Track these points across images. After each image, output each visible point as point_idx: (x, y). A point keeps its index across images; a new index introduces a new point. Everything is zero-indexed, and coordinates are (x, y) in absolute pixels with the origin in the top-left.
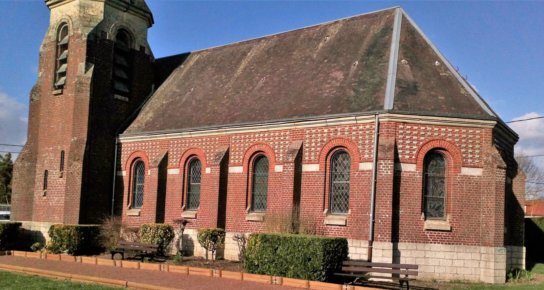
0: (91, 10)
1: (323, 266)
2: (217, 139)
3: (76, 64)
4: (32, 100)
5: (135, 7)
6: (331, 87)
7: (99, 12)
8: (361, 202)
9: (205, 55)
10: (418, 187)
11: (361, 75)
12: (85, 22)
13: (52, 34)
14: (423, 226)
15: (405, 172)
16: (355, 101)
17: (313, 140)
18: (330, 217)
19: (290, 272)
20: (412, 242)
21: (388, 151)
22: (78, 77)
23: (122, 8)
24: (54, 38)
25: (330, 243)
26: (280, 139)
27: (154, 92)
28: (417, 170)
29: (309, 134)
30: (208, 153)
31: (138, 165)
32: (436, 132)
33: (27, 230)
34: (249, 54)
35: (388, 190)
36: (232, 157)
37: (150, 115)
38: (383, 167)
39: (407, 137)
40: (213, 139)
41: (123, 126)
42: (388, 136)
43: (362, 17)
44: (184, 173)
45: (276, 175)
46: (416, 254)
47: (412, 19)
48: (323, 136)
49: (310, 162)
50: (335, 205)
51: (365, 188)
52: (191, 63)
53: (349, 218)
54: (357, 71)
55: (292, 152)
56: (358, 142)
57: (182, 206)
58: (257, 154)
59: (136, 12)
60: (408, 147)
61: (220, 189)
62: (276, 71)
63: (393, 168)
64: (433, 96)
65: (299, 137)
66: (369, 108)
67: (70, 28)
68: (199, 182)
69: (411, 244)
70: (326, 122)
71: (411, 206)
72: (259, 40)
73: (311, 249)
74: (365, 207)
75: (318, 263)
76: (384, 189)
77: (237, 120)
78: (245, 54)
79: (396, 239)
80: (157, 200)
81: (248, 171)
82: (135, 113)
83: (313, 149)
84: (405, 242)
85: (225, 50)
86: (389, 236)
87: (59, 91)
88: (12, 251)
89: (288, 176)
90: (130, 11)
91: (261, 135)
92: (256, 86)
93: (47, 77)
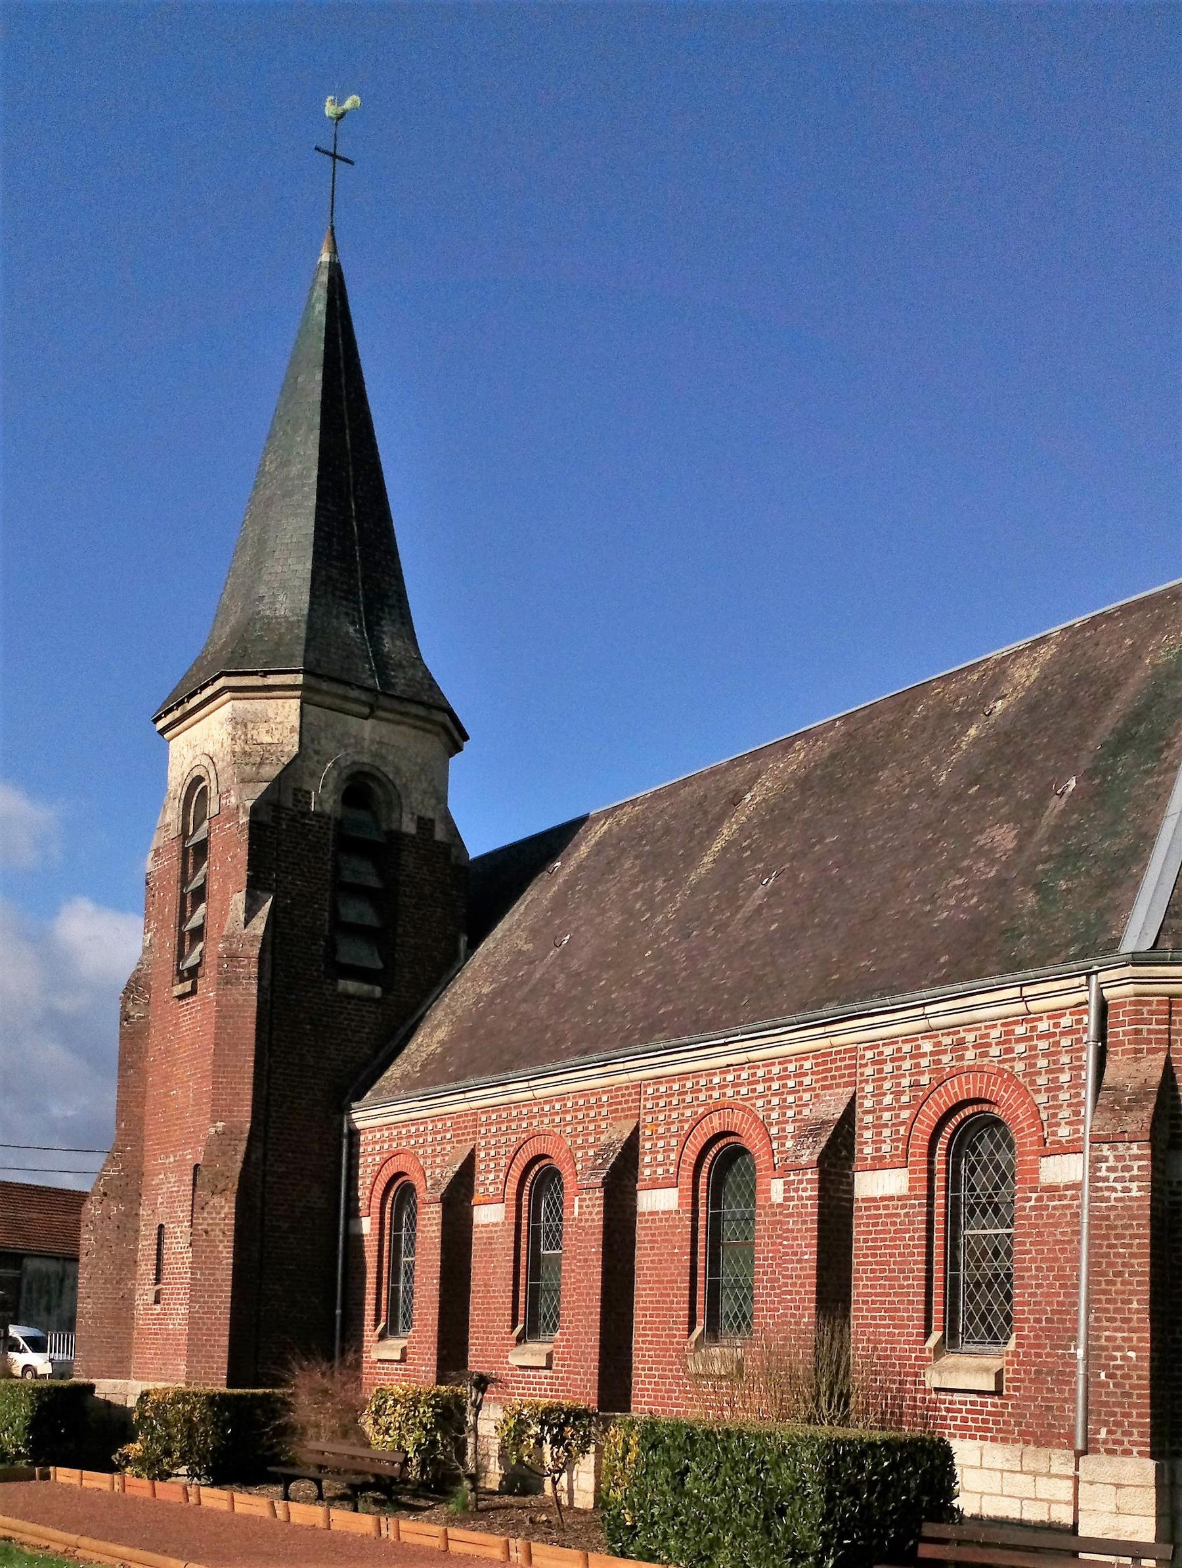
0: (263, 727)
1: (824, 1535)
2: (605, 1098)
3: (226, 900)
4: (126, 1017)
5: (398, 698)
6: (966, 886)
7: (286, 732)
8: (1049, 1303)
9: (625, 819)
11: (1078, 827)
12: (248, 768)
13: (172, 815)
16: (1033, 930)
17: (887, 1085)
18: (949, 1360)
21: (1129, 1109)
22: (227, 938)
24: (175, 830)
25: (863, 1454)
26: (785, 1086)
27: (467, 959)
30: (578, 1148)
31: (401, 1194)
33: (116, 1407)
34: (748, 796)
35: (1132, 1255)
36: (647, 1159)
37: (441, 1034)
38: (1109, 1169)
41: (359, 1080)
42: (1137, 1051)
43: (1126, 610)
45: (774, 1215)
48: (917, 1065)
49: (879, 1163)
50: (971, 1318)
52: (584, 850)
55: (815, 1129)
57: (514, 1327)
59: (402, 714)
61: (604, 1266)
62: (814, 845)
63: (1147, 1173)
65: (843, 1076)
66: (1072, 951)
67: (213, 793)
68: (558, 1246)
70: (925, 1017)
73: (786, 1473)
76: (1117, 1255)
77: (663, 1030)
78: (736, 799)
81: (930, 1205)
82: (402, 1031)
83: (887, 1115)
85: (684, 792)
86: (1141, 1434)
87: (187, 986)
88: (51, 1469)
89: (800, 1215)
90: (380, 713)
91: (730, 1077)
92: (741, 907)
93: (162, 947)
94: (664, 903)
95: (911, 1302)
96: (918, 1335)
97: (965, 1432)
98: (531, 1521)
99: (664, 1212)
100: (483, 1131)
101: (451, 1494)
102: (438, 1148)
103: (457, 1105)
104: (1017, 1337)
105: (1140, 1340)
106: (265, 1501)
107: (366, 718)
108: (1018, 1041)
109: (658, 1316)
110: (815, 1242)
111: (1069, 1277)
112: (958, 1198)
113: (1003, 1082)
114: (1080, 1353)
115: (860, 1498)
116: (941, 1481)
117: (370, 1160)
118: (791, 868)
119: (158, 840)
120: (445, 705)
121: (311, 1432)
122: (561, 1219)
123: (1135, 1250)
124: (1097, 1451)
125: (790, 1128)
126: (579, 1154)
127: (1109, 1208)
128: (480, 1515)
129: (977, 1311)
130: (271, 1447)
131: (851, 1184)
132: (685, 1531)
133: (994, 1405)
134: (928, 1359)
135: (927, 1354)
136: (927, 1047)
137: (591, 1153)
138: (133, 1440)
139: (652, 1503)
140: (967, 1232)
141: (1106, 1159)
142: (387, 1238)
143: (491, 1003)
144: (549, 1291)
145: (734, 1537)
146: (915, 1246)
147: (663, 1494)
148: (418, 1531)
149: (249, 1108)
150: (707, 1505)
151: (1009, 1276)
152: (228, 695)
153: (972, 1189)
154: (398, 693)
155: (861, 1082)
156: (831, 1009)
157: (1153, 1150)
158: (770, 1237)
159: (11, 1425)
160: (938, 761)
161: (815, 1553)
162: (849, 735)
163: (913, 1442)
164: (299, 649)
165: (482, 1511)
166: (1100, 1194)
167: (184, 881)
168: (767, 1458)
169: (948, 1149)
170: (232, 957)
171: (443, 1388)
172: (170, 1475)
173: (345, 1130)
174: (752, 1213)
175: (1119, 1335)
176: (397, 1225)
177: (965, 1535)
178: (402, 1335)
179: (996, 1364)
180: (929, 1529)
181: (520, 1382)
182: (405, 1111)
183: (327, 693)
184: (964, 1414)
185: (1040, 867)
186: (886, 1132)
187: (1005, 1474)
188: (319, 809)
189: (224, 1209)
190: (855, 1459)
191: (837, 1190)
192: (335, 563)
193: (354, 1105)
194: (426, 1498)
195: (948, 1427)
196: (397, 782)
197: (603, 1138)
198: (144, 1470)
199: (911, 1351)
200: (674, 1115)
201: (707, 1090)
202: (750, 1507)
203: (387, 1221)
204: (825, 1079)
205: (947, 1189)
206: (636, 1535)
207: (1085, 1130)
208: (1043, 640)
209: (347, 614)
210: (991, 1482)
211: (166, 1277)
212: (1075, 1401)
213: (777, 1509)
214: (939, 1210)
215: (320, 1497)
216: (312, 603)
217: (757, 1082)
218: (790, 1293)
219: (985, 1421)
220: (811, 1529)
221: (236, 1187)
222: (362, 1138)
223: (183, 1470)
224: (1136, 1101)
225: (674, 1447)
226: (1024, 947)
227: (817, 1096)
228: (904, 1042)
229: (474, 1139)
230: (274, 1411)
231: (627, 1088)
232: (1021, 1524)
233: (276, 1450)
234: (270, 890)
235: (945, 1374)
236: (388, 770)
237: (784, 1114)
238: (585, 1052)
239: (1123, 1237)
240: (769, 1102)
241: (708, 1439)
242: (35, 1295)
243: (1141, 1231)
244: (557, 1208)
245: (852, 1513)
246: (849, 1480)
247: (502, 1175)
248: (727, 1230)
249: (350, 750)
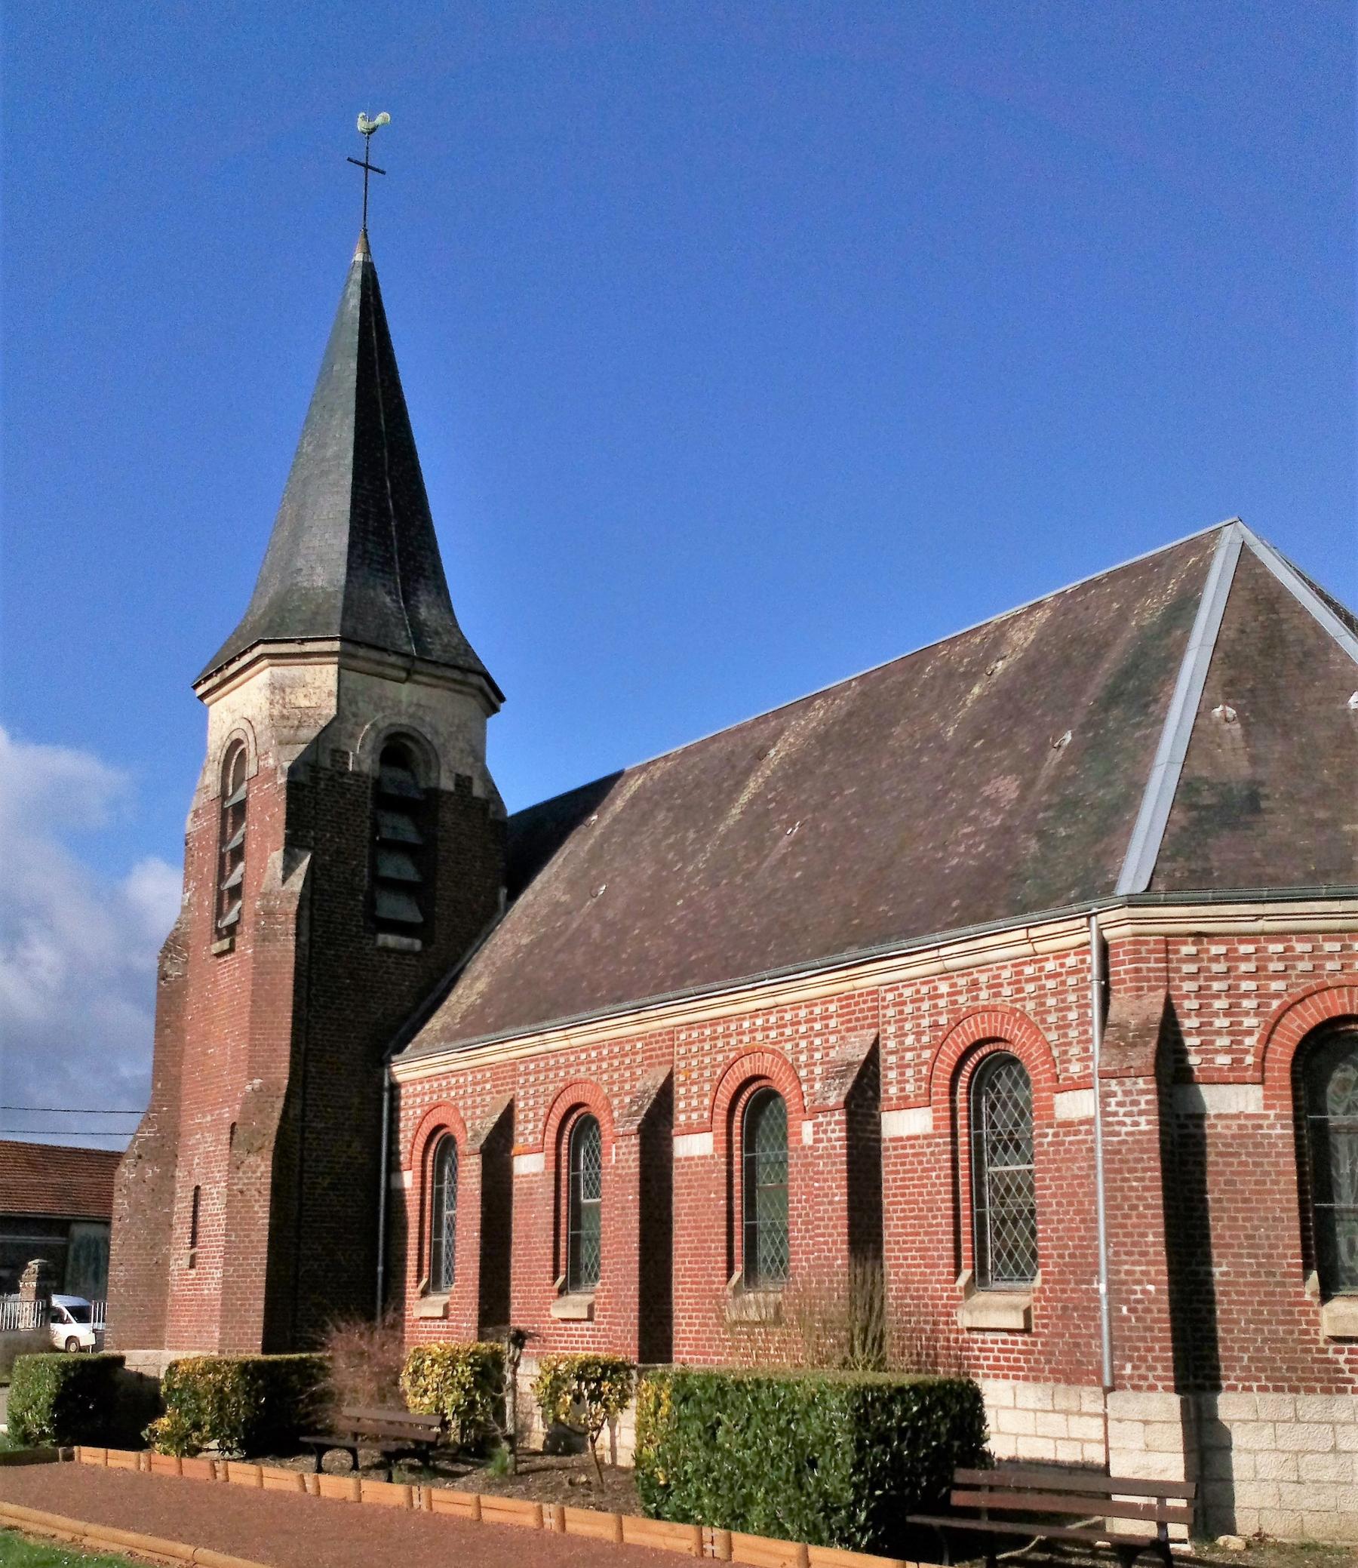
2: (639, 1045)
3: (264, 859)
4: (163, 976)
5: (434, 663)
6: (973, 834)
8: (1071, 1238)
9: (658, 774)
10: (1279, 1173)
13: (211, 778)
14: (1316, 1323)
15: (1219, 1116)
17: (908, 1026)
18: (980, 1298)
19: (756, 1515)
20: (1277, 1389)
21: (1134, 1045)
22: (265, 896)
23: (395, 673)
24: (215, 789)
25: (892, 1399)
26: (812, 1029)
27: (507, 910)
28: (1267, 1107)
29: (895, 1005)
31: (442, 1146)
32: (1331, 956)
34: (772, 752)
35: (1146, 1189)
36: (682, 1105)
37: (481, 986)
38: (1120, 1104)
39: (1216, 986)
40: (628, 1047)
41: (399, 1031)
44: (558, 1166)
45: (806, 1156)
46: (1293, 1437)
47: (1274, 547)
48: (935, 1006)
49: (905, 1104)
50: (999, 1256)
51: (1081, 1185)
52: (619, 804)
53: (1037, 1300)
54: (1061, 765)
56: (1043, 1021)
57: (555, 1278)
58: (752, 1088)
60: (1221, 1022)
62: (834, 797)
63: (1154, 1107)
64: (1322, 825)
65: (866, 1018)
66: (1073, 894)
67: (251, 755)
68: (598, 1195)
69: (1271, 1396)
71: (1259, 1247)
72: (808, 703)
75: (835, 1476)
76: (1131, 1189)
77: (693, 977)
78: (761, 755)
79: (1207, 1377)
80: (482, 1261)
81: (954, 1143)
82: (444, 983)
83: (909, 1055)
84: (1249, 1389)
85: (713, 748)
86: (1165, 1369)
87: (225, 944)
88: (76, 1448)
89: (829, 1156)
91: (759, 1022)
92: (767, 856)
93: (200, 905)
94: (694, 854)
95: (940, 1241)
96: (949, 1274)
97: (998, 1372)
98: (571, 1483)
99: (701, 1158)
100: (522, 1081)
101: (490, 1457)
102: (478, 1100)
103: (494, 1055)
104: (1043, 1273)
105: (1157, 1273)
106: (293, 1475)
107: (403, 682)
108: (1028, 981)
109: (696, 1262)
110: (844, 1183)
111: (1088, 1212)
112: (980, 1136)
113: (1016, 1021)
114: (1103, 1288)
115: (891, 1446)
116: (971, 1425)
117: (411, 1112)
118: (813, 819)
119: (198, 801)
120: (480, 669)
121: (348, 1397)
122: (600, 1167)
123: (1147, 1183)
124: (1123, 1387)
125: (818, 1070)
126: (616, 1102)
127: (1120, 1143)
128: (518, 1479)
129: (1027, 1240)
130: (308, 1415)
131: (879, 1124)
132: (718, 1488)
133: (1025, 1343)
134: (959, 1298)
135: (958, 1293)
136: (944, 988)
137: (627, 1100)
138: (161, 1413)
139: (685, 1459)
140: (991, 1169)
141: (1114, 1095)
142: (428, 1191)
143: (530, 953)
144: (590, 1240)
145: (767, 1493)
146: (942, 1185)
147: (695, 1449)
148: (451, 1500)
149: (287, 1064)
150: (739, 1460)
151: (1032, 1212)
152: (265, 662)
153: (994, 1126)
154: (434, 658)
155: (884, 1023)
156: (853, 953)
157: (1159, 1083)
158: (803, 1180)
159: (35, 1403)
160: (945, 717)
161: (847, 1507)
162: (864, 694)
163: (942, 1385)
164: (336, 618)
165: (522, 1473)
166: (1111, 1129)
167: (223, 841)
168: (797, 1407)
169: (969, 1088)
170: (269, 913)
171: (483, 1345)
172: (199, 1450)
173: (386, 1084)
174: (785, 1156)
175: (1138, 1268)
176: (439, 1177)
177: (996, 1481)
178: (444, 1290)
179: (1024, 1301)
180: (961, 1475)
181: (562, 1335)
182: (446, 1063)
184: (996, 1354)
185: (1041, 815)
186: (909, 1072)
187: (1039, 1414)
189: (262, 1167)
190: (884, 1406)
191: (865, 1131)
192: (370, 537)
193: (394, 1058)
194: (466, 1463)
195: (981, 1367)
197: (638, 1084)
198: (171, 1446)
199: (943, 1290)
200: (707, 1060)
201: (738, 1034)
202: (781, 1460)
203: (429, 1174)
204: (849, 1021)
205: (969, 1127)
206: (670, 1494)
207: (1094, 1066)
208: (1038, 605)
209: (384, 585)
210: (1024, 1423)
211: (201, 1240)
212: (1100, 1337)
213: (809, 1461)
214: (963, 1148)
215: (355, 1467)
216: (348, 574)
217: (785, 1026)
218: (823, 1235)
219: (1017, 1360)
220: (842, 1481)
221: (273, 1145)
222: (403, 1091)
223: (214, 1444)
224: (1140, 1036)
225: (706, 1401)
226: (1029, 890)
227: (842, 1038)
228: (923, 983)
229: (513, 1089)
230: (311, 1376)
231: (660, 1034)
232: (1056, 1466)
233: (313, 1418)
234: (309, 848)
235: (976, 1314)
236: (426, 731)
237: (812, 1057)
238: (620, 1000)
239: (1135, 1170)
240: (797, 1045)
241: (738, 1389)
242: (82, 1262)
243: (1152, 1164)
244: (595, 1155)
245: (883, 1462)
246: (878, 1428)
247: (541, 1125)
248: (762, 1173)
249: (388, 712)
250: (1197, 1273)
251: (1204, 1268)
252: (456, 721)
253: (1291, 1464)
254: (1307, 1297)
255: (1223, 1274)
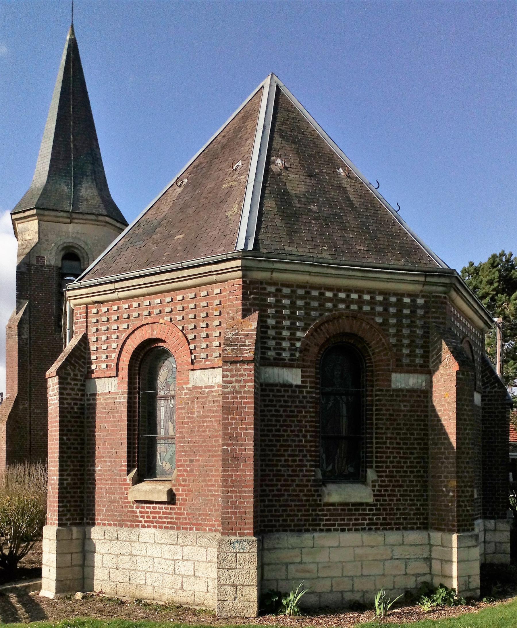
0: (27, 233)
5: (81, 213)
15: (101, 394)
74: (295, 461)
154: (81, 211)
183: (48, 215)
188: (48, 264)
196: (86, 248)
234: (26, 299)
250: (89, 470)
251: (92, 468)
252: (97, 238)
253: (114, 560)
254: (128, 482)
255: (99, 470)
